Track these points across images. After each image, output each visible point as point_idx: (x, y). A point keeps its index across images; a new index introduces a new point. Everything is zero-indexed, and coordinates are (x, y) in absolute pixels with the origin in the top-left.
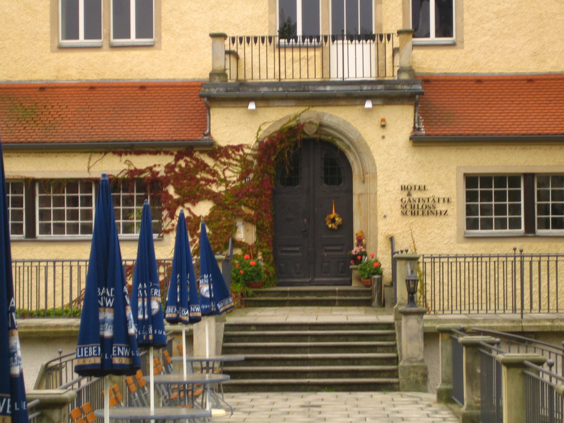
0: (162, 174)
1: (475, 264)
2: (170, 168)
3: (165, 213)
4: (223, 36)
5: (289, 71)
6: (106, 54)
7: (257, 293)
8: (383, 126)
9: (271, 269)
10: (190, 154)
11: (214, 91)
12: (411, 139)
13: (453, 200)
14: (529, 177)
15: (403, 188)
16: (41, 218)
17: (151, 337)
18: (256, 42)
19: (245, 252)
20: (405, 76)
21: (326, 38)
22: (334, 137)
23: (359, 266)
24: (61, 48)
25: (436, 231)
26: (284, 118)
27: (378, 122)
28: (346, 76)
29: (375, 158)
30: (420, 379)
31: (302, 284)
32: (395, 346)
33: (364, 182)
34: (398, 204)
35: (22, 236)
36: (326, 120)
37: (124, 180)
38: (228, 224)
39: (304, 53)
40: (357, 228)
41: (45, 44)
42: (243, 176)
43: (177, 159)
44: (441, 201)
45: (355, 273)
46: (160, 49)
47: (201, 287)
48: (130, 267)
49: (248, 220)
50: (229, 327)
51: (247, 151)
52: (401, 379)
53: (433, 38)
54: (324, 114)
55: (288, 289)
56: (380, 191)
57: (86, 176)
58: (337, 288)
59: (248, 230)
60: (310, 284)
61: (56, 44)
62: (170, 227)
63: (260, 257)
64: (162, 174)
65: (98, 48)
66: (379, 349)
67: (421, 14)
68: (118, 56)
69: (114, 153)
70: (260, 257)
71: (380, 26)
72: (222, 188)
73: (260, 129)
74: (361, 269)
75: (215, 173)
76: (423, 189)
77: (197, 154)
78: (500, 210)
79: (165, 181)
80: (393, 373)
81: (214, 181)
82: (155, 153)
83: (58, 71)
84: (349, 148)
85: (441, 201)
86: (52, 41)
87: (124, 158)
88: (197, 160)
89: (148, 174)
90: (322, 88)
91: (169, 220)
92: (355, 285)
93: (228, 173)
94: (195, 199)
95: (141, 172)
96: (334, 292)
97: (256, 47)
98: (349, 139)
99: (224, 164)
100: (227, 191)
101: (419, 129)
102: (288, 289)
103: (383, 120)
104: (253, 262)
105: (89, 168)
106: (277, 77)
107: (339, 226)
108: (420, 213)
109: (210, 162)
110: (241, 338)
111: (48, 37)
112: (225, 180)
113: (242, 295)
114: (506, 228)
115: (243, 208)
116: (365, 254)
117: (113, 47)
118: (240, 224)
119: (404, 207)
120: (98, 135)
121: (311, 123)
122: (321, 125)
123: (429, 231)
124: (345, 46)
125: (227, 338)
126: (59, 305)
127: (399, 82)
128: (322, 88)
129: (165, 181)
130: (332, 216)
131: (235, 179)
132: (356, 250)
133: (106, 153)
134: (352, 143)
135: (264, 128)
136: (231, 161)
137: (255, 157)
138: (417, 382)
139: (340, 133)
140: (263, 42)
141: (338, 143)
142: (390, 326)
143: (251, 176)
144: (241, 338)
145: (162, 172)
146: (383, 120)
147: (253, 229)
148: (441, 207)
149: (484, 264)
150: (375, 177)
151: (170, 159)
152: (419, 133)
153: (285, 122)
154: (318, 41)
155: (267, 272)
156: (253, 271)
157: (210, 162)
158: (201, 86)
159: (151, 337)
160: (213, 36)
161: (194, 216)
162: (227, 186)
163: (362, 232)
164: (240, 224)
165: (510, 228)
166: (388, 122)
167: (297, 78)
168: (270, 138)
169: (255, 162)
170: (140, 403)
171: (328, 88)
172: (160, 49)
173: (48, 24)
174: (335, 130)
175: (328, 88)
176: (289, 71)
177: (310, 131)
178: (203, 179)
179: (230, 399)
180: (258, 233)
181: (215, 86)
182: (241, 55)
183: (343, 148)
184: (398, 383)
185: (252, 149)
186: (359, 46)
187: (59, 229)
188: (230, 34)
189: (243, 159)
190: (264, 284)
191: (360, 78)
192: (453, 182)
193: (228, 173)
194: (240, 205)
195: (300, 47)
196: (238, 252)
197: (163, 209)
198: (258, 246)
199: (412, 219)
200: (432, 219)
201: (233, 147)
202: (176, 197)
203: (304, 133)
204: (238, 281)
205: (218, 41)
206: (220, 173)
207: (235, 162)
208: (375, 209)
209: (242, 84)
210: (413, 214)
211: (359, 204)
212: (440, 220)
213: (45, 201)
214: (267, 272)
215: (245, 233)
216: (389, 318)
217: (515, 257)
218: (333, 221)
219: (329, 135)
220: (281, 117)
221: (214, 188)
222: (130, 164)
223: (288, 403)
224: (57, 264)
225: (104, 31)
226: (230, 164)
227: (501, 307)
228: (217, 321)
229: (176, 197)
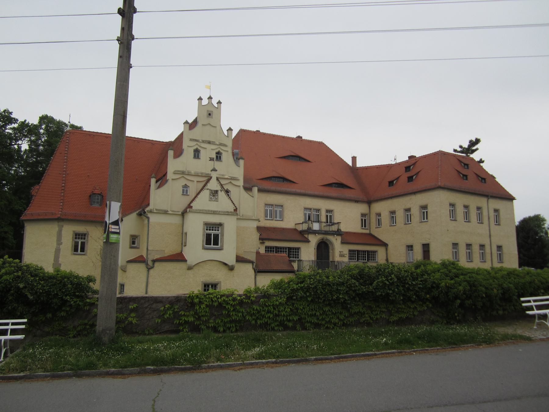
14: (368, 251)
15: (340, 252)
16: (287, 251)
27: (335, 239)
47: (26, 226)
67: (533, 269)
68: (277, 222)
76: (342, 252)
114: (211, 245)
119: (340, 255)
148: (345, 256)
165: (213, 245)
166: (337, 239)
170: (455, 248)
187: (298, 255)
210: (341, 257)
212: (345, 258)
224: (119, 230)
228: (255, 228)
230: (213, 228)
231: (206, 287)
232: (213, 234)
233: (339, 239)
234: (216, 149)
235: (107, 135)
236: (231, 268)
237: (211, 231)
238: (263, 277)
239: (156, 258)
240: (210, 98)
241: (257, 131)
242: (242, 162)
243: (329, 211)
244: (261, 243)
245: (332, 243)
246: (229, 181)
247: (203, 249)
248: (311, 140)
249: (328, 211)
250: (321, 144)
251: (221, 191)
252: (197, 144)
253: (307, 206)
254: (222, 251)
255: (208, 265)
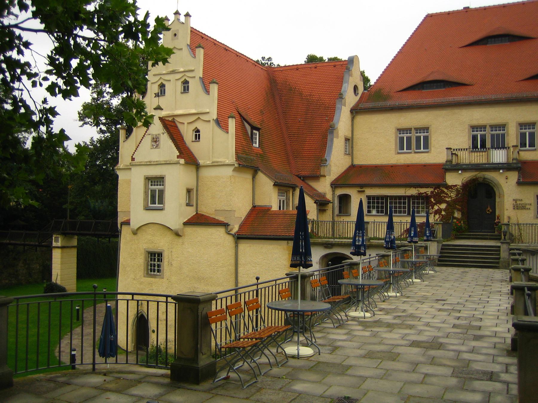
0: (429, 194)
1: (530, 227)
2: (432, 192)
3: (430, 207)
4: (451, 149)
5: (476, 160)
6: (413, 155)
7: (461, 235)
8: (507, 179)
9: (467, 227)
10: (439, 188)
11: (447, 167)
12: (516, 183)
13: (533, 204)
15: (514, 200)
17: (389, 246)
18: (462, 150)
19: (457, 221)
20: (515, 161)
21: (489, 148)
22: (489, 182)
23: (497, 227)
24: (399, 153)
25: (526, 215)
26: (472, 176)
27: (505, 177)
28: (493, 161)
29: (504, 189)
30: (507, 265)
31: (477, 232)
32: (500, 253)
33: (500, 198)
34: (512, 206)
35: (406, 214)
36: (486, 176)
37: (417, 196)
38: (451, 211)
39: (481, 154)
40: (497, 214)
41: (393, 152)
42: (457, 195)
43: (434, 190)
44: (528, 204)
45: (496, 229)
46: (431, 153)
48: (418, 225)
49: (458, 210)
50: (443, 245)
51: (458, 187)
52: (500, 265)
53: (422, 150)
54: (485, 174)
55: (472, 233)
56: (505, 201)
57: (405, 195)
58: (489, 234)
59: (458, 213)
60: (480, 232)
61: (397, 152)
62: (432, 212)
63: (462, 223)
64: (429, 194)
65: (411, 153)
66: (494, 255)
68: (417, 155)
69: (414, 187)
70: (462, 223)
71: (508, 144)
72: (450, 199)
73: (463, 180)
74: (498, 227)
75: (447, 194)
77: (441, 188)
78: (400, 207)
79: (430, 197)
80: (498, 263)
81: (447, 197)
82: (427, 188)
83: (397, 161)
84: (494, 186)
85: (528, 204)
86: (395, 151)
87: (417, 189)
88: (441, 190)
89: (425, 194)
90: (484, 166)
91: (431, 209)
92: (496, 233)
93: (452, 194)
94: (440, 203)
95: (423, 193)
96: (488, 235)
97: (464, 152)
98: (494, 183)
99: (451, 191)
100: (451, 200)
101: (520, 179)
102: (472, 233)
103: (507, 176)
104: (459, 224)
105: (405, 192)
106: (469, 162)
107: (491, 213)
108: (520, 208)
109: (446, 190)
110: (447, 249)
111: (394, 150)
112: (450, 197)
113: (455, 235)
115: (457, 206)
116: (500, 222)
117: (415, 153)
118: (455, 211)
119: (514, 206)
120: (408, 182)
121: (481, 177)
122: (484, 178)
123: (523, 215)
124: (493, 151)
125: (442, 249)
126: (383, 237)
127: (513, 163)
128: (484, 166)
129: (430, 197)
130: (488, 209)
131: (454, 196)
132: (497, 221)
133: (411, 187)
134: (495, 184)
135: (464, 179)
136: (453, 190)
137: (461, 189)
138: (506, 266)
139: (491, 181)
140: (462, 150)
141: (490, 184)
142: (499, 247)
143: (460, 195)
144: (447, 249)
145: (429, 193)
146: (507, 176)
147: (460, 213)
148: (528, 207)
149: (534, 227)
150: (504, 196)
151: (432, 190)
152: (520, 181)
153: (472, 177)
154: (486, 150)
155: (464, 228)
156: (460, 227)
157: (446, 190)
158: (443, 165)
159: (389, 246)
160: (447, 149)
161: (440, 208)
162: (451, 198)
163: (499, 215)
164: (455, 211)
166: (509, 177)
167: (476, 162)
168: (467, 182)
169: (461, 191)
171: (487, 166)
172: (431, 153)
173: (394, 146)
174: (490, 180)
175: (487, 166)
176: (476, 160)
177: (481, 180)
178: (443, 196)
179: (437, 269)
180: (461, 214)
181: (448, 165)
182: (459, 155)
183: (493, 186)
184: (499, 266)
185: (460, 186)
186: (498, 151)
188: (453, 148)
189: (457, 190)
190: (463, 232)
191: (498, 162)
192: (533, 198)
193: (452, 194)
194: (456, 205)
195: (480, 152)
196: (455, 221)
197: (429, 206)
198: (462, 219)
199: (517, 211)
200: (524, 211)
201: (453, 185)
202: (434, 202)
203: (478, 181)
204: (455, 230)
205: (449, 150)
206: (449, 194)
207: (454, 191)
208: (504, 207)
209: (458, 164)
210: (517, 209)
211: (498, 205)
212: (528, 211)
213: (414, 203)
214: (464, 228)
215: (457, 215)
216: (499, 244)
217: (407, 223)
218: (489, 211)
219: (488, 181)
220: (470, 175)
221: (447, 199)
222: (419, 191)
223: (458, 271)
225: (412, 147)
226: (452, 191)
227: (534, 242)
229: (434, 202)
230: (155, 182)
231: (159, 257)
232: (158, 190)
233: (514, 176)
234: (182, 77)
235: (292, 67)
236: (177, 234)
237: (156, 187)
238: (249, 245)
239: (124, 220)
240: (177, 13)
241: (465, 8)
242: (214, 89)
243: (500, 127)
244: (359, 191)
245: (499, 186)
246: (196, 117)
247: (144, 210)
248: (503, 4)
249: (522, 125)
250: (429, 17)
251: (163, 133)
252: (161, 77)
253: (475, 123)
254: (163, 211)
255: (150, 230)
